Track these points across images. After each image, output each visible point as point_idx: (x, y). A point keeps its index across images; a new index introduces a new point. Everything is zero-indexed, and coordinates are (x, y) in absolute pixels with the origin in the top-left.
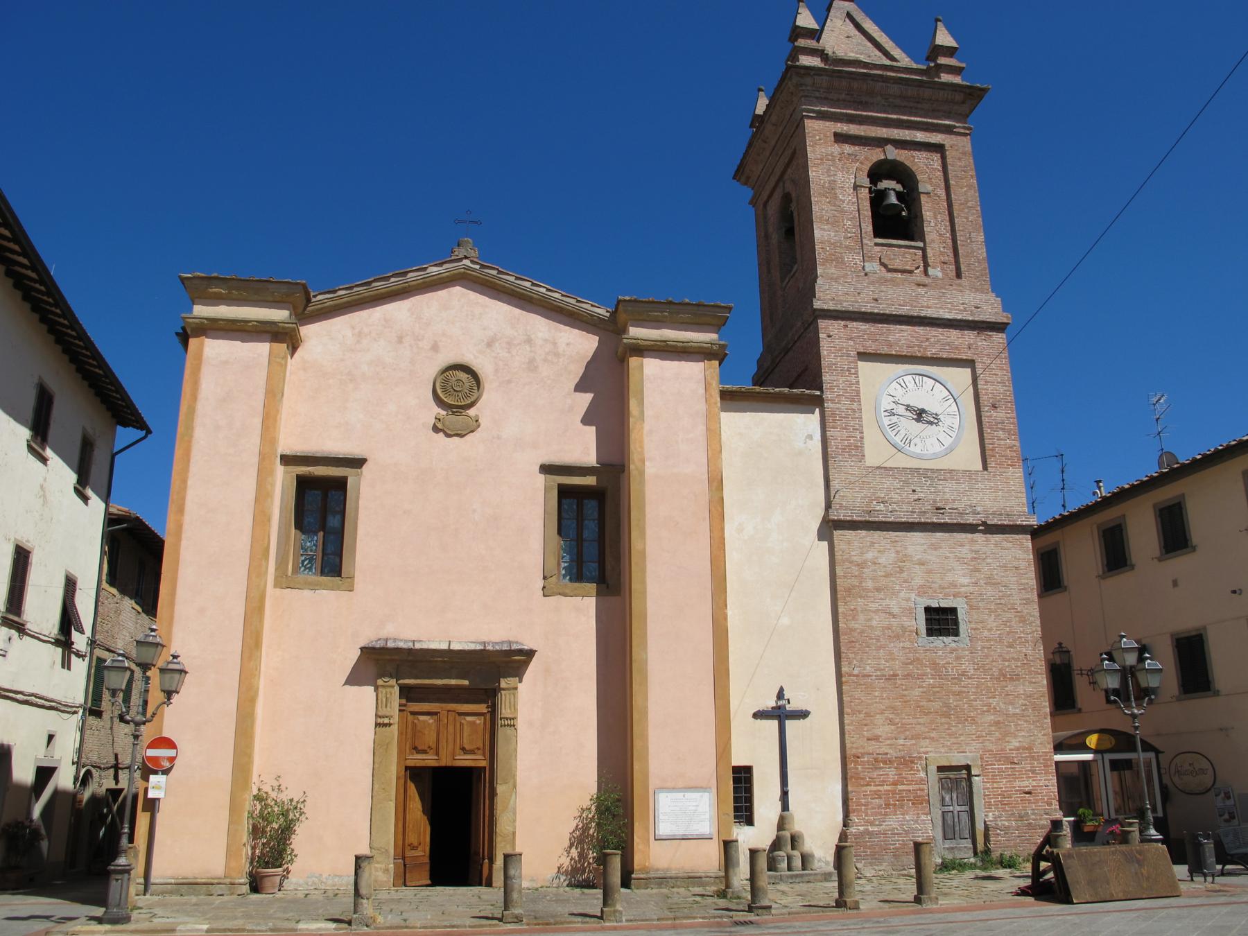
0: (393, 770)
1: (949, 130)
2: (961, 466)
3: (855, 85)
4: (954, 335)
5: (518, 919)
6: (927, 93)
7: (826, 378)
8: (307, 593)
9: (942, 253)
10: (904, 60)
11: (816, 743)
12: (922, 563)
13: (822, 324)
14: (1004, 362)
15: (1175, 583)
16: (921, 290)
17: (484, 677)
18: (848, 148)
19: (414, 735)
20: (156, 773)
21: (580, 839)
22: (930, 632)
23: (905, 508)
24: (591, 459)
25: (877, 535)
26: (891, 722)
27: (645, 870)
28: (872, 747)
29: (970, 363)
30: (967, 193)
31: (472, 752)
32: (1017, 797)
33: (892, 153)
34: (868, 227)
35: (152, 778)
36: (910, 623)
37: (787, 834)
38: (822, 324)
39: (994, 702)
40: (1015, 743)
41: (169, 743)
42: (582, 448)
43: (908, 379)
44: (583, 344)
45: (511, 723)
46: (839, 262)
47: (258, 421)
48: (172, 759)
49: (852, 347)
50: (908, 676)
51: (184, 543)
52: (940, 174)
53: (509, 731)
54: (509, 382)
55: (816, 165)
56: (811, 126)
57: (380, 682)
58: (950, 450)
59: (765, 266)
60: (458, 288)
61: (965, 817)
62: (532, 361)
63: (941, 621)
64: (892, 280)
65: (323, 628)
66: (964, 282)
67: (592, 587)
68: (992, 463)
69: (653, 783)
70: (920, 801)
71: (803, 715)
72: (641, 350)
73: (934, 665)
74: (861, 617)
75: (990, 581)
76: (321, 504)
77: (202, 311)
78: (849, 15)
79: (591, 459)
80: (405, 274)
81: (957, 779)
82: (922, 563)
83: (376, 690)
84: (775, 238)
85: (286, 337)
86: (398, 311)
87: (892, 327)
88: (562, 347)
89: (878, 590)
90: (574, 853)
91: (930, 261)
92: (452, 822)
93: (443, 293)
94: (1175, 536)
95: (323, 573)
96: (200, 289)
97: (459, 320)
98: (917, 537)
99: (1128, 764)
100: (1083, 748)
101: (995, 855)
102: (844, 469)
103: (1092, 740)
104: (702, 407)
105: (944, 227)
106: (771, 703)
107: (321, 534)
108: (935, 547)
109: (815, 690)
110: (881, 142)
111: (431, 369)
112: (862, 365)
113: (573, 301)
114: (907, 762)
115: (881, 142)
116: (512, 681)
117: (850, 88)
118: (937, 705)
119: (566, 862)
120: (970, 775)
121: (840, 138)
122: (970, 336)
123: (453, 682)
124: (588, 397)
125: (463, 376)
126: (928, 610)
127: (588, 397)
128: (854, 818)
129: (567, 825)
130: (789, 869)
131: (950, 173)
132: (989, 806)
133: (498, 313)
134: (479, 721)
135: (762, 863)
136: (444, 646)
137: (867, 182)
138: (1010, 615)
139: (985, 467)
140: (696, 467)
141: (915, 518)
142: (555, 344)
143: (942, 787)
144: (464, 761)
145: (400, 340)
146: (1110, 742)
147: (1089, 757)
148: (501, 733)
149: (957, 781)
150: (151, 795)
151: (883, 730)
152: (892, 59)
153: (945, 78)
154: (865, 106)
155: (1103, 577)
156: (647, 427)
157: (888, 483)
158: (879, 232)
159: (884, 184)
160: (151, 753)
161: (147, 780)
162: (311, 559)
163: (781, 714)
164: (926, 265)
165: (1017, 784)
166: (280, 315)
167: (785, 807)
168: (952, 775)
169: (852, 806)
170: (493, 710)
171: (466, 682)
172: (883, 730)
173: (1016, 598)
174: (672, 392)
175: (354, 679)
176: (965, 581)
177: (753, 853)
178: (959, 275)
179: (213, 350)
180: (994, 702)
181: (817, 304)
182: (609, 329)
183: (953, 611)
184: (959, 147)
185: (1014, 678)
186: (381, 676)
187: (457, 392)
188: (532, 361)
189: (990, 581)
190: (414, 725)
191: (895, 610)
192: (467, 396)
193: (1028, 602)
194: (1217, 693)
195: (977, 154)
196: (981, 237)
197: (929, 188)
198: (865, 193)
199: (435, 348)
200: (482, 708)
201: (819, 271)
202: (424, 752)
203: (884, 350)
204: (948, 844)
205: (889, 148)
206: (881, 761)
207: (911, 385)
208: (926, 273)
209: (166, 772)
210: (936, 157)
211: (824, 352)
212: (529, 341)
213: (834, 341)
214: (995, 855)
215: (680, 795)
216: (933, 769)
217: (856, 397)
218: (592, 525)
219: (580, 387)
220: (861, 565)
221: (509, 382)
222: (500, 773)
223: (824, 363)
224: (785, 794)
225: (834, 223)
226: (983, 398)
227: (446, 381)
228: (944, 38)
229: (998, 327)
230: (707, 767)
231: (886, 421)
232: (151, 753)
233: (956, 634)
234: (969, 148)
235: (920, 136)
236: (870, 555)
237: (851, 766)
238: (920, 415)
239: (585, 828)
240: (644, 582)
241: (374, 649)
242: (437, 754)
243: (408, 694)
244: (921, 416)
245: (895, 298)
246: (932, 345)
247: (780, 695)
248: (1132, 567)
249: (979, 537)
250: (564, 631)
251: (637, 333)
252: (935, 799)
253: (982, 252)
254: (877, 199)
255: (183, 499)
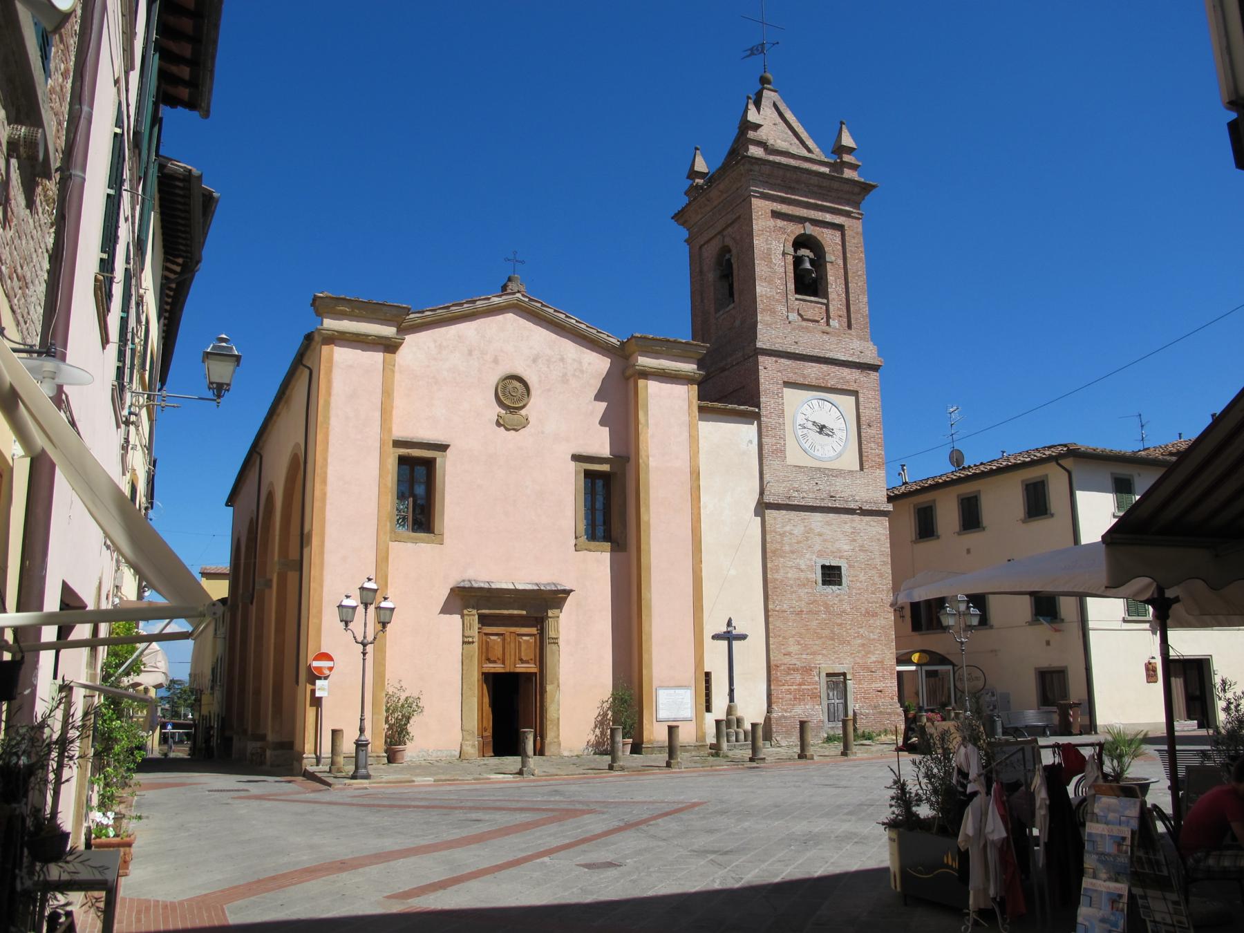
0: (475, 676)
1: (847, 214)
2: (847, 467)
3: (788, 174)
4: (846, 372)
5: (622, 769)
6: (836, 185)
7: (763, 399)
8: (410, 545)
9: (839, 309)
10: (818, 154)
11: (751, 656)
12: (820, 535)
13: (761, 359)
14: (877, 395)
15: (968, 551)
16: (826, 337)
17: (536, 608)
18: (780, 223)
19: (487, 649)
20: (320, 678)
21: (601, 722)
22: (824, 583)
23: (811, 495)
24: (605, 452)
25: (793, 514)
26: (799, 644)
27: (650, 742)
28: (787, 660)
29: (855, 393)
30: (857, 265)
31: (527, 662)
32: (873, 694)
33: (810, 229)
34: (791, 286)
35: (318, 682)
36: (812, 576)
37: (734, 718)
38: (761, 359)
39: (861, 631)
40: (873, 658)
41: (327, 657)
42: (600, 443)
43: (815, 402)
44: (599, 365)
45: (555, 641)
46: (773, 312)
47: (378, 414)
48: (331, 669)
49: (780, 377)
50: (810, 612)
51: (328, 507)
52: (840, 248)
53: (554, 647)
54: (549, 390)
55: (759, 235)
56: (756, 203)
57: (465, 612)
58: (840, 455)
59: (697, 294)
60: (511, 315)
61: (841, 706)
62: (565, 375)
63: (831, 575)
64: (806, 328)
65: (422, 575)
66: (853, 332)
67: (608, 545)
68: (866, 465)
69: (655, 683)
70: (815, 696)
71: (743, 637)
72: (646, 374)
73: (826, 606)
74: (782, 571)
75: (862, 549)
76: (417, 487)
77: (330, 324)
78: (775, 105)
79: (605, 452)
80: (474, 302)
81: (838, 681)
82: (820, 535)
83: (463, 616)
84: (711, 276)
85: (390, 346)
86: (468, 329)
87: (807, 364)
88: (585, 366)
89: (793, 552)
90: (598, 731)
91: (831, 315)
92: (512, 710)
93: (500, 318)
94: (971, 518)
95: (414, 530)
96: (322, 307)
97: (510, 340)
98: (818, 516)
99: (935, 673)
100: (910, 662)
101: (860, 732)
102: (772, 464)
103: (915, 657)
104: (686, 418)
105: (841, 289)
106: (724, 629)
107: (411, 499)
108: (829, 524)
109: (751, 622)
110: (801, 220)
111: (493, 379)
112: (788, 392)
113: (563, 316)
114: (807, 670)
115: (801, 220)
116: (556, 611)
117: (786, 179)
118: (827, 632)
119: (592, 738)
120: (845, 679)
121: (776, 215)
122: (856, 374)
123: (516, 612)
124: (604, 405)
125: (517, 384)
126: (823, 567)
127: (604, 405)
128: (774, 706)
129: (592, 714)
130: (737, 740)
131: (848, 246)
132: (856, 700)
133: (540, 336)
134: (532, 640)
135: (760, 732)
136: (511, 587)
137: (791, 250)
138: (874, 572)
139: (862, 469)
140: (683, 463)
141: (818, 503)
142: (580, 363)
143: (828, 687)
144: (521, 668)
145: (470, 353)
146: (926, 658)
147: (913, 668)
148: (549, 649)
149: (836, 684)
150: (318, 694)
151: (794, 649)
152: (809, 150)
153: (848, 174)
154: (792, 190)
155: (915, 542)
156: (650, 431)
157: (801, 477)
158: (798, 290)
159: (804, 252)
160: (316, 664)
161: (314, 684)
162: (404, 519)
163: (729, 637)
164: (828, 317)
165: (873, 686)
166: (389, 331)
167: (732, 699)
168: (834, 679)
169: (774, 699)
170: (542, 632)
171: (524, 612)
172: (794, 649)
173: (878, 561)
174: (667, 405)
175: (446, 610)
176: (846, 547)
177: (754, 726)
178: (849, 326)
179: (341, 355)
180: (861, 631)
181: (759, 345)
182: (621, 355)
183: (839, 568)
184: (854, 227)
185: (875, 615)
186: (467, 607)
187: (512, 395)
188: (565, 375)
189: (862, 549)
190: (487, 643)
191: (803, 567)
192: (520, 400)
193: (885, 563)
194: (991, 627)
195: (865, 233)
196: (866, 299)
197: (833, 258)
198: (790, 259)
199: (496, 361)
200: (534, 630)
201: (759, 318)
202: (494, 662)
203: (800, 380)
204: (831, 725)
205: (807, 224)
206: (792, 669)
207: (816, 407)
208: (828, 324)
209: (326, 678)
210: (838, 234)
211: (762, 380)
212: (562, 360)
213: (769, 372)
214: (860, 732)
215: (672, 691)
216: (823, 675)
217: (781, 414)
218: (610, 502)
219: (599, 397)
220: (782, 535)
221: (549, 390)
222: (549, 677)
223: (762, 388)
224: (731, 691)
225: (770, 281)
226: (863, 419)
227: (505, 387)
228: (847, 140)
229: (875, 368)
230: (688, 673)
231: (800, 433)
232: (316, 664)
233: (840, 584)
234: (860, 229)
235: (828, 217)
236: (788, 528)
237: (773, 672)
238: (822, 429)
239: (605, 715)
240: (649, 544)
241: (464, 588)
242: (503, 663)
243: (484, 620)
244: (820, 429)
245: (810, 342)
246: (832, 378)
247: (729, 623)
248: (938, 537)
249: (856, 517)
250: (589, 575)
251: (644, 361)
252: (824, 696)
253: (866, 310)
254: (798, 261)
255: (326, 473)
